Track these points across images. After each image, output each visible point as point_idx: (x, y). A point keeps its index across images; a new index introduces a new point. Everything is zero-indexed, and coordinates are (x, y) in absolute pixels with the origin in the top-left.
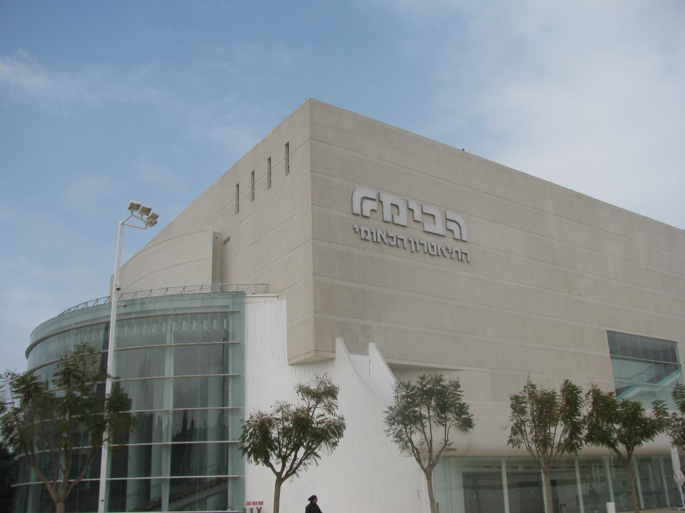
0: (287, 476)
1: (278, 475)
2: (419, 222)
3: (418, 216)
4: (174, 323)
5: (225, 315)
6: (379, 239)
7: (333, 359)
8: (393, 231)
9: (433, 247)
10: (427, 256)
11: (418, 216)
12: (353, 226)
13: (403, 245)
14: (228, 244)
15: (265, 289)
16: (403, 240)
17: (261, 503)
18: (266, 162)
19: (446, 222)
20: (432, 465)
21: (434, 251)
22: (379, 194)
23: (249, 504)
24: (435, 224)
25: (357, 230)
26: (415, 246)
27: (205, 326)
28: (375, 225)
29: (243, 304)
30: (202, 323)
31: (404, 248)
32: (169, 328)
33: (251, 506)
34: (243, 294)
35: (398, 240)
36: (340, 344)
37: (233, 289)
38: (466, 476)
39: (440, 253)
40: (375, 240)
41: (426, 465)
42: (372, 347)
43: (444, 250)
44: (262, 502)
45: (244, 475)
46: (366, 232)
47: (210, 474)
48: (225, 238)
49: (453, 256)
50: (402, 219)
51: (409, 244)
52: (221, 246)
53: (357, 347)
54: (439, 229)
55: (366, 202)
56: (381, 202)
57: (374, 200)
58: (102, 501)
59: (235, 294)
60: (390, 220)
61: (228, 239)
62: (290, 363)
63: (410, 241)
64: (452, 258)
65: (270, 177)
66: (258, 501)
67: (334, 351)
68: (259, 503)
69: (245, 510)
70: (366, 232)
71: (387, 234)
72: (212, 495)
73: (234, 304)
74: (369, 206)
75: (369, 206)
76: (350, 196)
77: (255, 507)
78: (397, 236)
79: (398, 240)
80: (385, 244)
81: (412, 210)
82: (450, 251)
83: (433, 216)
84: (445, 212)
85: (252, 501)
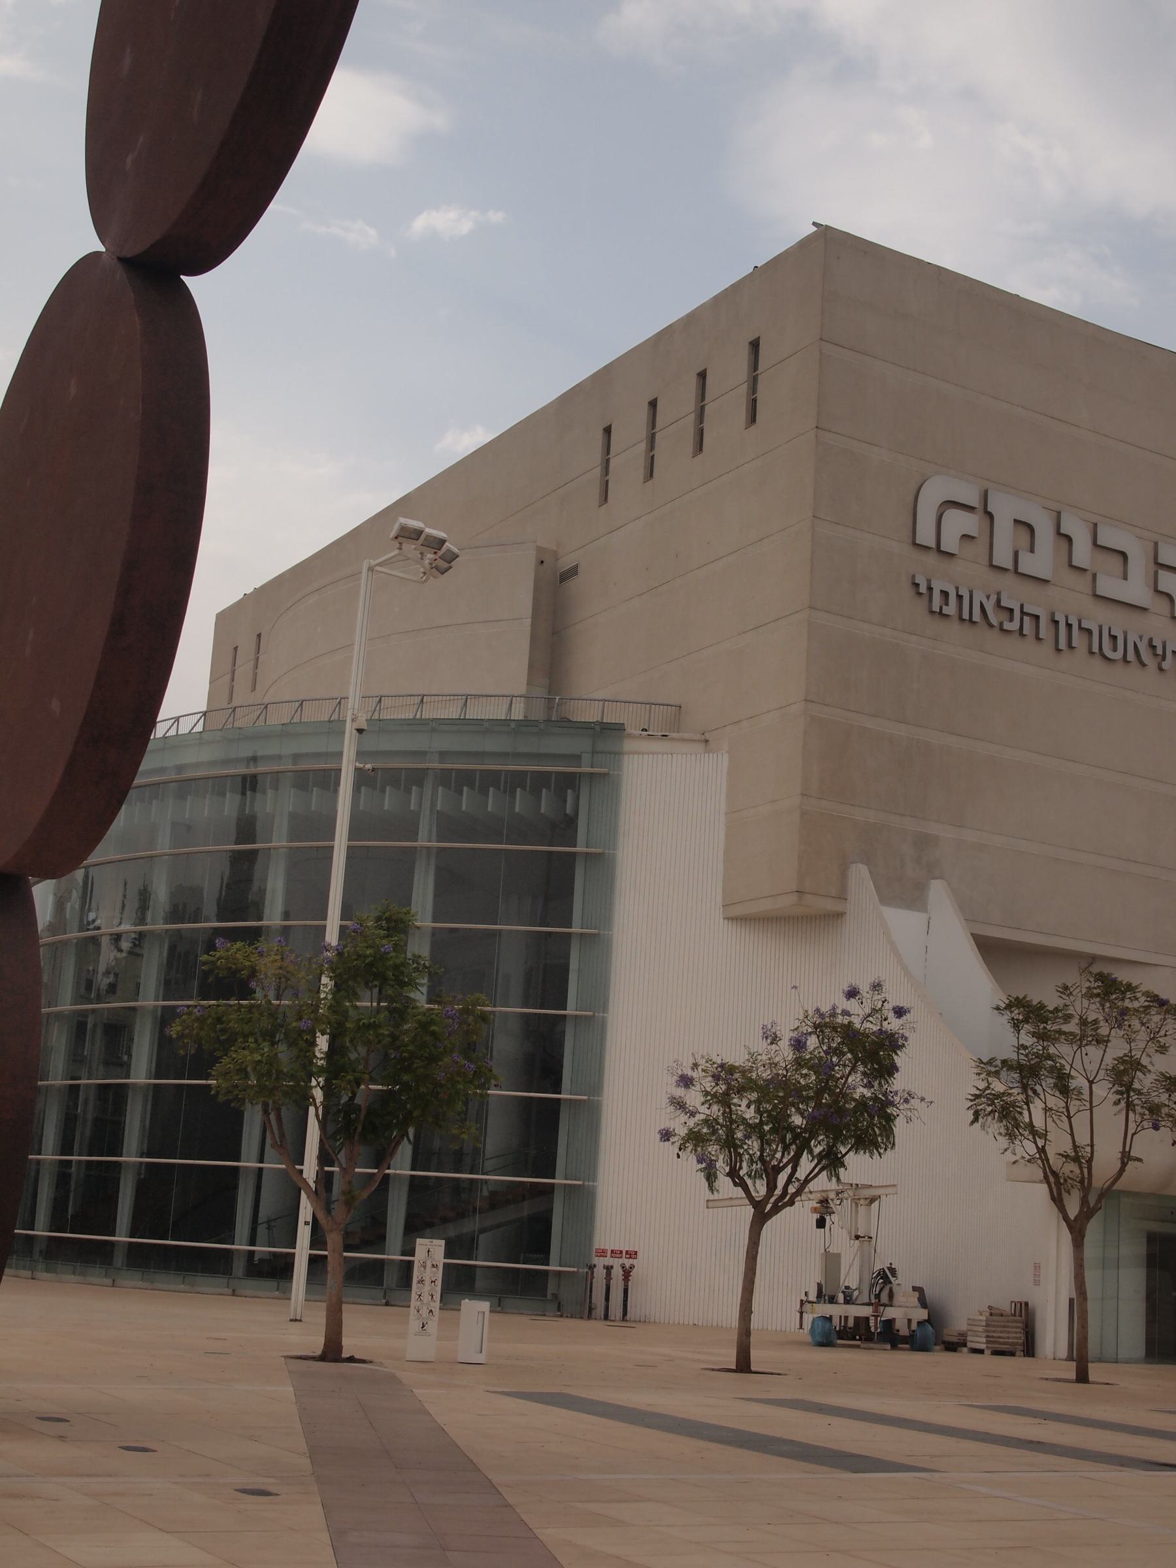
0: (776, 1209)
1: (757, 1205)
2: (1085, 570)
3: (1082, 553)
4: (440, 789)
5: (569, 782)
6: (977, 616)
7: (840, 915)
8: (1015, 594)
9: (1114, 638)
10: (1097, 661)
11: (1082, 553)
12: (914, 577)
13: (1037, 628)
14: (572, 583)
15: (673, 724)
16: (1037, 617)
17: (632, 1255)
18: (693, 381)
19: (1156, 573)
20: (1087, 1213)
21: (1115, 649)
22: (986, 492)
23: (602, 1253)
24: (1125, 578)
25: (923, 589)
26: (1063, 634)
27: (520, 803)
28: (967, 575)
29: (618, 754)
30: (513, 796)
31: (1038, 639)
32: (427, 804)
33: (608, 1261)
34: (616, 730)
35: (1026, 619)
36: (860, 874)
37: (589, 714)
38: (1152, 1239)
39: (1131, 656)
40: (966, 616)
41: (1073, 1210)
42: (937, 891)
43: (1143, 647)
44: (636, 1253)
45: (594, 1180)
46: (945, 594)
47: (494, 1171)
48: (566, 563)
49: (1165, 665)
50: (1039, 562)
51: (1052, 627)
52: (555, 587)
53: (908, 893)
54: (1135, 590)
55: (952, 515)
56: (990, 516)
57: (970, 509)
58: (306, 1223)
59: (598, 728)
60: (1009, 564)
61: (573, 571)
62: (739, 911)
63: (1056, 623)
64: (1161, 669)
65: (701, 422)
66: (625, 1248)
67: (842, 897)
68: (612, 1251)
69: (592, 1267)
70: (945, 594)
71: (999, 601)
72: (491, 1228)
73: (594, 752)
74: (958, 524)
75: (958, 524)
76: (911, 498)
77: (616, 1263)
78: (1022, 606)
79: (1026, 619)
80: (991, 626)
81: (1069, 539)
82: (1159, 651)
83: (1124, 555)
84: (1156, 544)
85: (609, 1247)
